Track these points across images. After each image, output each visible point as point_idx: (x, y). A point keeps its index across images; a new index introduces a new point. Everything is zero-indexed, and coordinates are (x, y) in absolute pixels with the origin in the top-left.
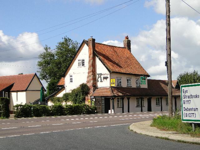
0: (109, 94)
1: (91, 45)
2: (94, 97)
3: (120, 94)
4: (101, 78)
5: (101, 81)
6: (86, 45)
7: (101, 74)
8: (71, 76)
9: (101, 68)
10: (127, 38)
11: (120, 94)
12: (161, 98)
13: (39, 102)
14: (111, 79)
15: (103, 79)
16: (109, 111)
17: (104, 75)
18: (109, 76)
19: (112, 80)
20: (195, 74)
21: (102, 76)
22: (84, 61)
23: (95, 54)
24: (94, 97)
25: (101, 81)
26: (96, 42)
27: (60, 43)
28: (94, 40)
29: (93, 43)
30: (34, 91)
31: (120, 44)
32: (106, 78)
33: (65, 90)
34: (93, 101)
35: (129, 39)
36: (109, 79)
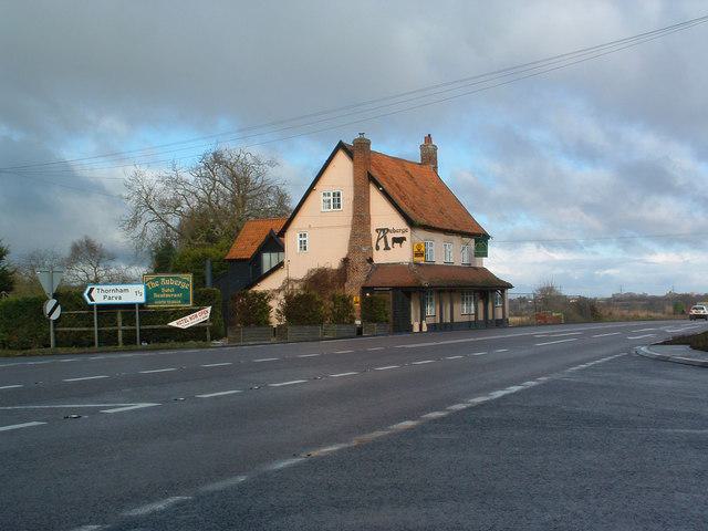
5: (387, 248)
10: (428, 139)
17: (394, 231)
21: (390, 236)
22: (339, 195)
32: (399, 240)
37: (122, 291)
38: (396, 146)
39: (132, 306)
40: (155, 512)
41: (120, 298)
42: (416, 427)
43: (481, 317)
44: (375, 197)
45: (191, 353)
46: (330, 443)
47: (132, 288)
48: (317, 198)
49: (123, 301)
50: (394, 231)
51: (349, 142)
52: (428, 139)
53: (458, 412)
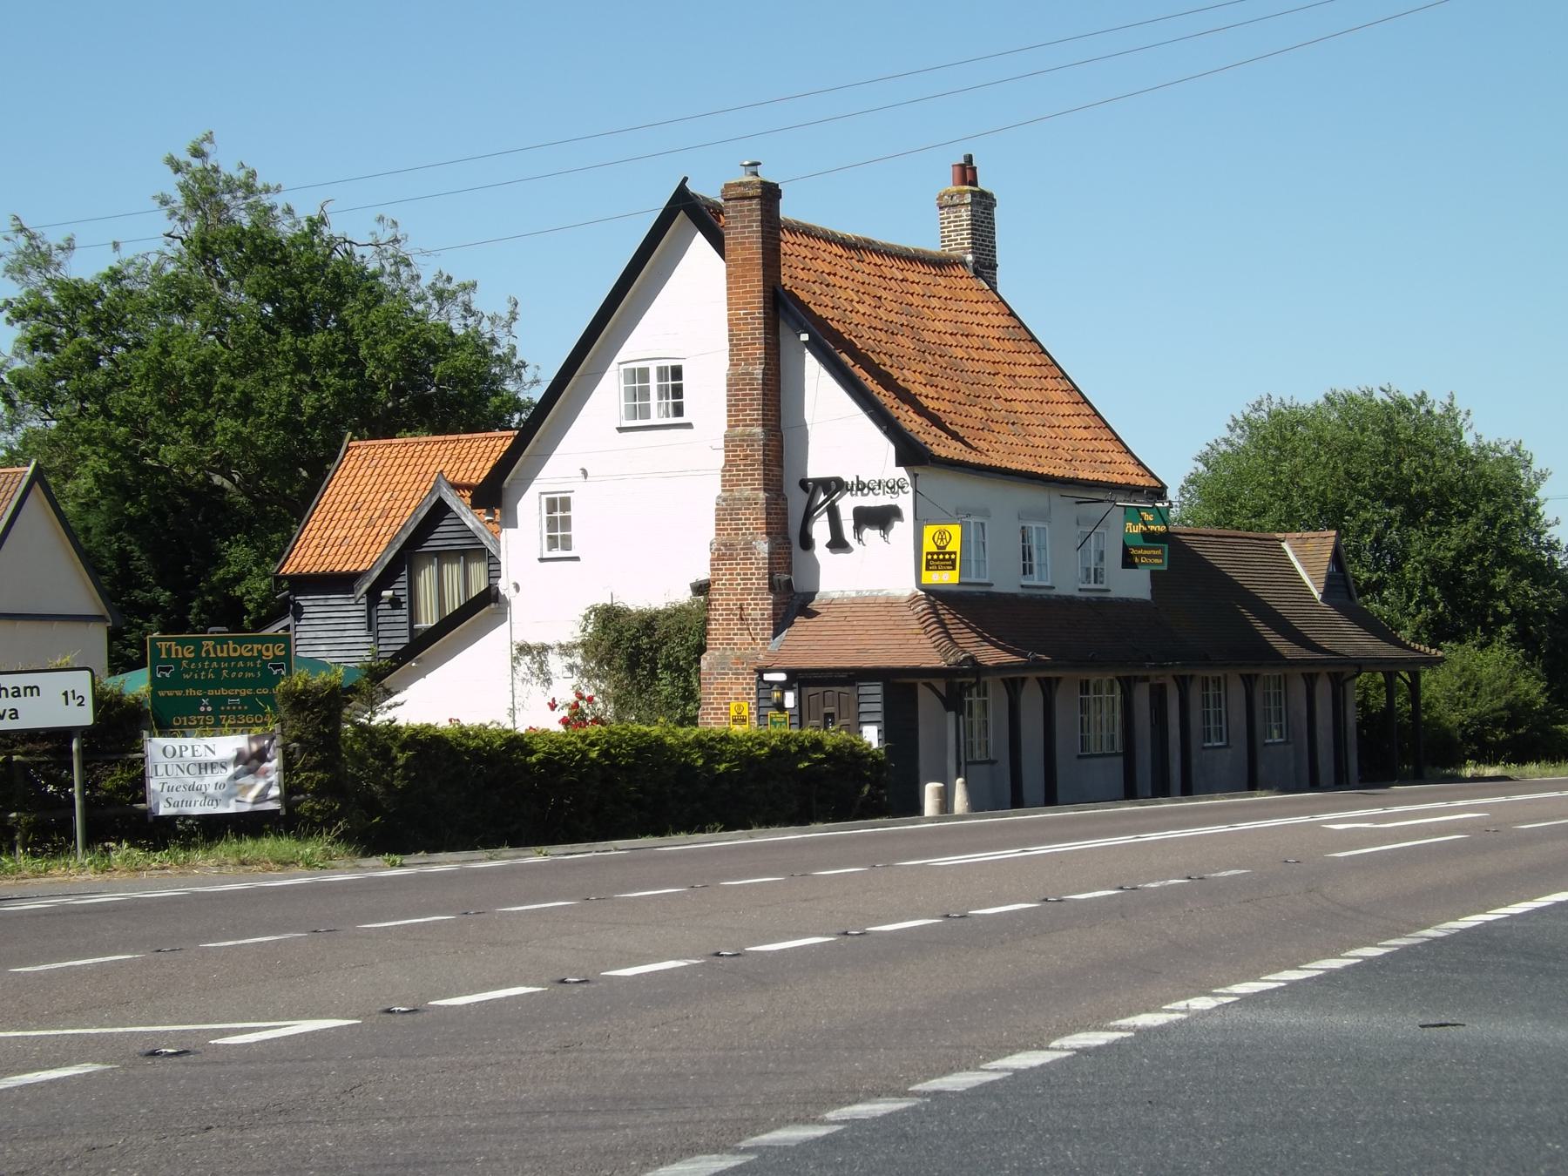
0: (920, 650)
1: (744, 229)
2: (788, 671)
3: (990, 655)
4: (834, 514)
5: (838, 543)
6: (700, 244)
7: (834, 486)
8: (558, 507)
9: (840, 437)
10: (967, 172)
11: (990, 655)
12: (1183, 683)
13: (801, 766)
14: (920, 522)
15: (858, 528)
16: (930, 790)
17: (861, 487)
18: (905, 502)
19: (930, 531)
20: (1399, 485)
21: (847, 505)
22: (677, 372)
23: (783, 320)
24: (788, 671)
25: (838, 543)
26: (788, 210)
27: (111, 268)
28: (770, 194)
29: (749, 221)
30: (19, 624)
31: (930, 229)
32: (881, 518)
33: (507, 624)
34: (780, 707)
35: (983, 184)
36: (903, 530)
37: (17, 693)
38: (868, 194)
39: (61, 736)
40: (1513, 916)
41: (15, 714)
42: (907, 1110)
43: (863, 707)
44: (823, 399)
45: (211, 873)
46: (874, 1095)
47: (52, 684)
48: (606, 398)
49: (25, 722)
50: (861, 487)
51: (707, 188)
52: (967, 172)
53: (784, 1150)
